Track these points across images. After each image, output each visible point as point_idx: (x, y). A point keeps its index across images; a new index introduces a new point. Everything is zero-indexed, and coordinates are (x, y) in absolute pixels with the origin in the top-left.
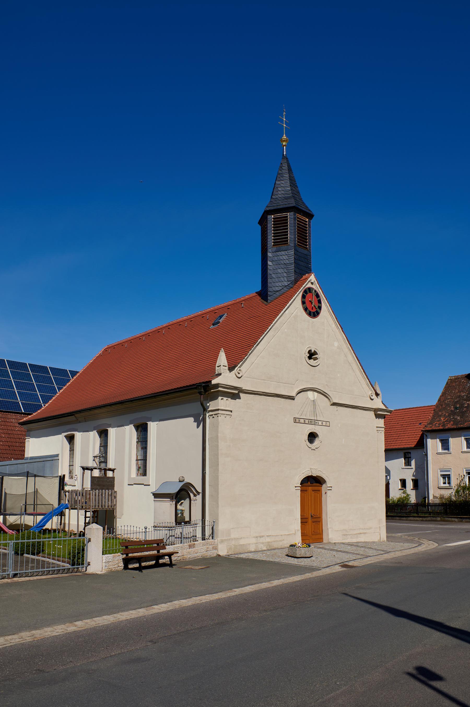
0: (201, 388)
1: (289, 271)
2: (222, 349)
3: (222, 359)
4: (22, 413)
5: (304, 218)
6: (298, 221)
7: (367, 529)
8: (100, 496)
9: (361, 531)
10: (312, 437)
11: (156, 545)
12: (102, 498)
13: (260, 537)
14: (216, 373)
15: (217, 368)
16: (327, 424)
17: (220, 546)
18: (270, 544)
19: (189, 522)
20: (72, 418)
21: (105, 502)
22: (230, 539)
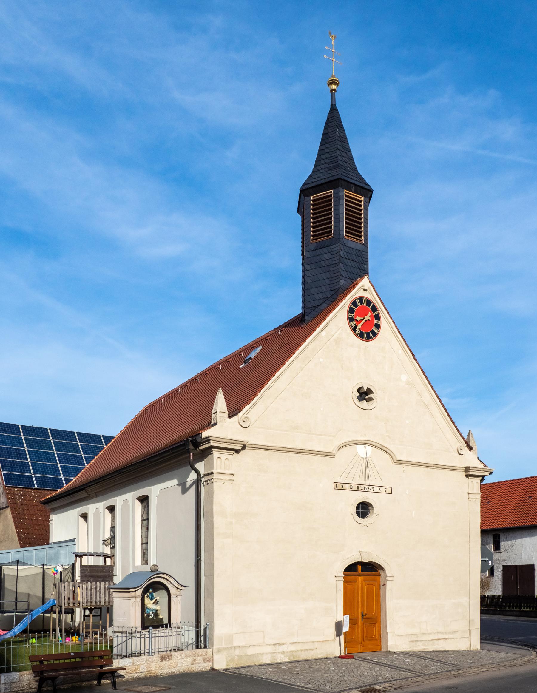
0: (189, 444)
1: (333, 276)
2: (220, 389)
3: (220, 403)
4: (36, 489)
5: (357, 196)
6: (347, 201)
7: (450, 633)
8: (94, 591)
9: (441, 636)
10: (363, 510)
11: (38, 663)
12: (96, 592)
13: (280, 644)
14: (212, 423)
15: (213, 415)
16: (388, 491)
17: (216, 657)
18: (294, 654)
19: (169, 625)
20: (83, 494)
21: (100, 597)
22: (231, 648)
